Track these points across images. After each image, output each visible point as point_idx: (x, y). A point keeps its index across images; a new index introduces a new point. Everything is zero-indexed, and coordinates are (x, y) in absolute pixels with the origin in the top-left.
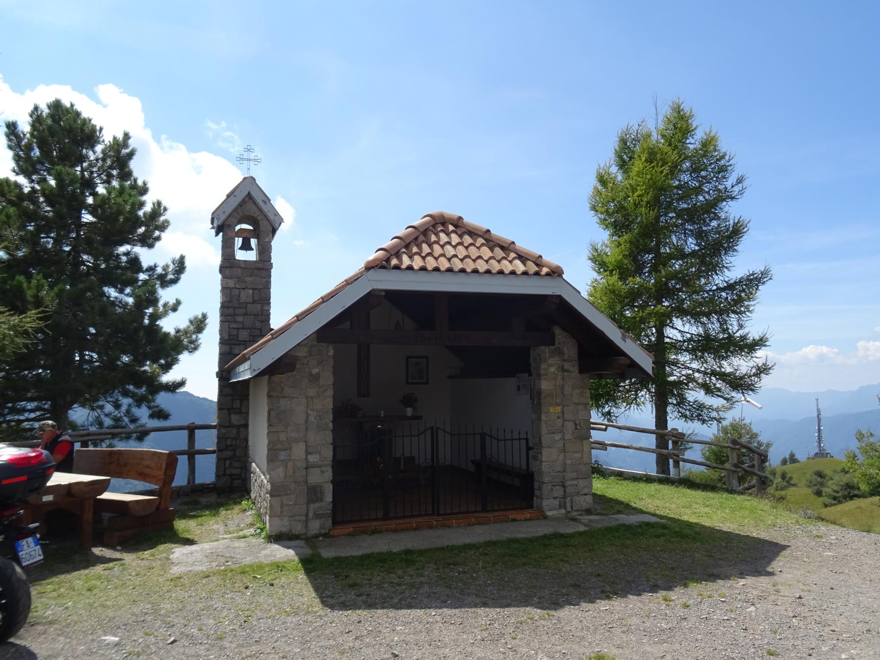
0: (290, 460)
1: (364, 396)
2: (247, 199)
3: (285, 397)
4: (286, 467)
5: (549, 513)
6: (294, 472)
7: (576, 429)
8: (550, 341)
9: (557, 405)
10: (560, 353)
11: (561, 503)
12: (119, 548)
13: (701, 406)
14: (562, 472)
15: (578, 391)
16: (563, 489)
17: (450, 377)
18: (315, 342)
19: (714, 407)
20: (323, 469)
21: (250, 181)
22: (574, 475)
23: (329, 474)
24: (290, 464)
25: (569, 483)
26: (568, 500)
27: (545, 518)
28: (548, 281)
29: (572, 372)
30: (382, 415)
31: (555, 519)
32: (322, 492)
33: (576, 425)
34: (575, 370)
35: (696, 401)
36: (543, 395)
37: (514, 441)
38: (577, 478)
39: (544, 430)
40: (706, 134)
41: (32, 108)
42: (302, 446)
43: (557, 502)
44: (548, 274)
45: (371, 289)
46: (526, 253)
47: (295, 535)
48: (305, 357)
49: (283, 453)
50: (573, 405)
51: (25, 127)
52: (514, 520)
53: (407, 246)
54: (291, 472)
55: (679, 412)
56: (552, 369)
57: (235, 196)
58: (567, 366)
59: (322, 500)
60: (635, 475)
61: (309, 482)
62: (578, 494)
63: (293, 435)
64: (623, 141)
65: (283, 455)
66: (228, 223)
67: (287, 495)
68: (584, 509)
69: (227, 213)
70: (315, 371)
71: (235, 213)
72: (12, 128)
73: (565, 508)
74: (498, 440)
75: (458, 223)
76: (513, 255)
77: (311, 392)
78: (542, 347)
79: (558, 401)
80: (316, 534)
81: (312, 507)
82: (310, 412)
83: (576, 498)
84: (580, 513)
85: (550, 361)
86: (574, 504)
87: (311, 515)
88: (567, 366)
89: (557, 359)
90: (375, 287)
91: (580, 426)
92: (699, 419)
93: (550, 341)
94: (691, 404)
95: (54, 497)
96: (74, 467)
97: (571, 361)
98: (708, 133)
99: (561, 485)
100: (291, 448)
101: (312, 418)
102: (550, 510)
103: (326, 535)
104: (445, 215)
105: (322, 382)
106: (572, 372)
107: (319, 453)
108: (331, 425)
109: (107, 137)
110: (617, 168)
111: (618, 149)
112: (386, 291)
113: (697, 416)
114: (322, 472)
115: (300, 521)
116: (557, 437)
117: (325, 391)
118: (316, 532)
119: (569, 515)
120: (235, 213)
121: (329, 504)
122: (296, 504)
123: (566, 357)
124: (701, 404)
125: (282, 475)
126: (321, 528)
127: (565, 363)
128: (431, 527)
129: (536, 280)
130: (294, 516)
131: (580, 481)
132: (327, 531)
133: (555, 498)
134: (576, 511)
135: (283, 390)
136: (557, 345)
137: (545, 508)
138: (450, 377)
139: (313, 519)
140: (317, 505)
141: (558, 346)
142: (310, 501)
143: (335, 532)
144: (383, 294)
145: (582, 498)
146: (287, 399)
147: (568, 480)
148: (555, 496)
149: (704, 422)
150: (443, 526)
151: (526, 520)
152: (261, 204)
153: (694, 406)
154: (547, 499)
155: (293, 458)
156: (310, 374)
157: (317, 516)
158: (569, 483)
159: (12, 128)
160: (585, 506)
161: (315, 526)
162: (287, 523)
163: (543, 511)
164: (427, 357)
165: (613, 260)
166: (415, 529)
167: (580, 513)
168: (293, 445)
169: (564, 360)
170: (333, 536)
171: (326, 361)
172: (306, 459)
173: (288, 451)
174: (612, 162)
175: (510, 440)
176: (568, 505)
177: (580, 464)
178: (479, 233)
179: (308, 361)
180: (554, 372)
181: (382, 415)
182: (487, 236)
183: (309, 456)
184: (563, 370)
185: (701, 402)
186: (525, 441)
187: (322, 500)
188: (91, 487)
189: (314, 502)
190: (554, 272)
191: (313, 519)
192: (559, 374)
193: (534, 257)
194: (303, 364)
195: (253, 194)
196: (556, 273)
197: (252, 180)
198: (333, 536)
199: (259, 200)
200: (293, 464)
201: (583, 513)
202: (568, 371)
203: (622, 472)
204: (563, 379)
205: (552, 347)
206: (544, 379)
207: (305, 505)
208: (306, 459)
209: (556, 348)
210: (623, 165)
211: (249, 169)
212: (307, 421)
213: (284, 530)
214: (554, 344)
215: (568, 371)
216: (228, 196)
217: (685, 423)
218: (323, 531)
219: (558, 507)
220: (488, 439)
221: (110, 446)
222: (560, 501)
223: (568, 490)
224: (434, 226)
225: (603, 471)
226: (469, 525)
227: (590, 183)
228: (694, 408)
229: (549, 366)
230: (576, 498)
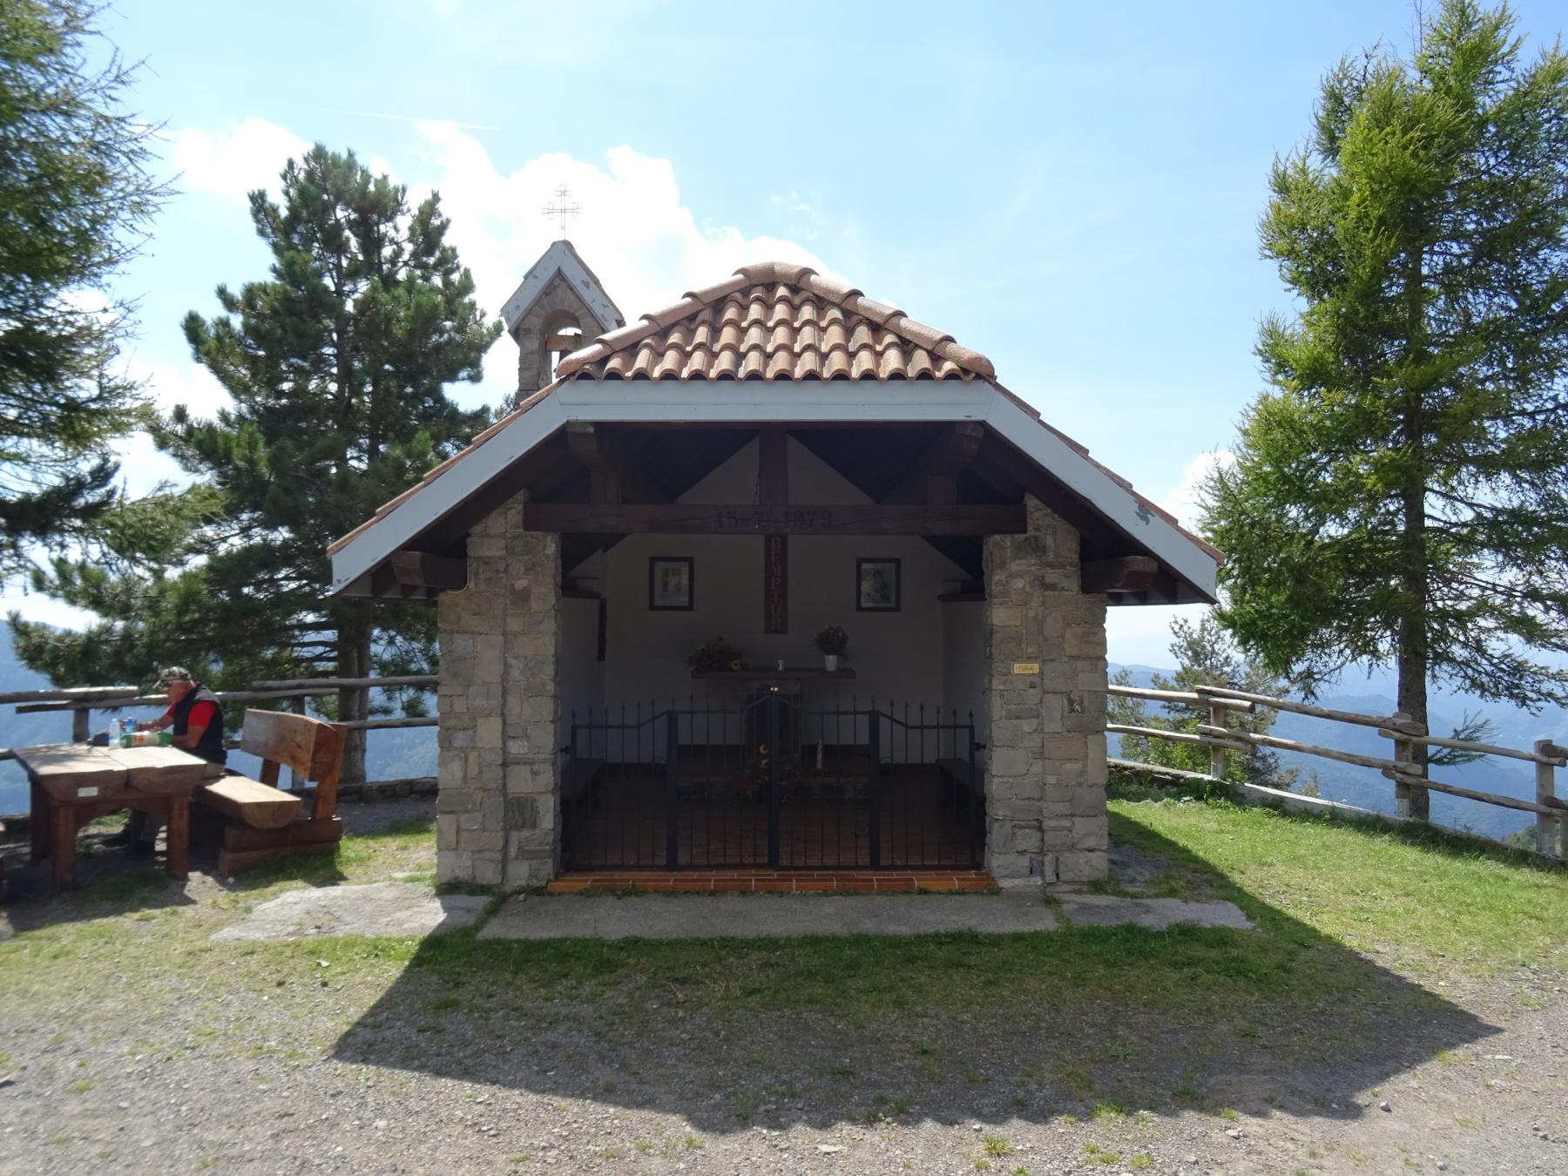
0: (474, 748)
1: (776, 632)
2: (557, 282)
3: (465, 632)
4: (466, 760)
5: (1005, 884)
6: (480, 772)
7: (1072, 710)
8: (1018, 524)
9: (1030, 659)
10: (1038, 548)
11: (1035, 863)
12: (231, 880)
13: (1519, 669)
14: (1038, 800)
15: (1079, 630)
16: (1039, 835)
17: (943, 598)
18: (521, 530)
19: (1550, 671)
20: (535, 767)
21: (564, 248)
22: (1064, 808)
23: (547, 778)
24: (473, 756)
25: (1053, 823)
26: (1049, 858)
27: (996, 892)
28: (954, 390)
29: (1063, 589)
30: (781, 668)
31: (1019, 897)
32: (535, 812)
33: (1071, 702)
34: (1073, 585)
35: (1507, 656)
36: (996, 638)
37: (926, 731)
38: (1072, 815)
39: (997, 707)
40: (1544, 56)
41: (284, 166)
42: (496, 723)
43: (1024, 862)
44: (951, 376)
45: (564, 421)
46: (917, 334)
47: (483, 886)
48: (501, 558)
49: (460, 735)
50: (1065, 659)
51: (279, 201)
52: (923, 892)
53: (664, 334)
54: (476, 771)
55: (1466, 677)
56: (1019, 584)
57: (535, 277)
58: (1052, 576)
59: (534, 826)
60: (1309, 807)
61: (510, 791)
62: (1072, 848)
63: (477, 703)
64: (1335, 97)
65: (460, 740)
66: (523, 326)
67: (466, 811)
68: (1086, 879)
69: (523, 308)
70: (521, 584)
71: (537, 308)
72: (259, 203)
73: (1042, 874)
74: (907, 727)
75: (799, 286)
76: (889, 338)
77: (514, 624)
78: (997, 537)
79: (1030, 650)
80: (522, 887)
81: (515, 836)
82: (512, 662)
83: (1066, 857)
84: (1077, 887)
85: (1014, 567)
86: (1062, 867)
87: (513, 851)
88: (1052, 576)
89: (1033, 561)
90: (573, 418)
91: (1081, 704)
92: (1511, 696)
93: (1018, 524)
94: (1495, 661)
95: (100, 791)
96: (314, 732)
97: (1063, 566)
98: (1551, 52)
99: (1034, 827)
100: (475, 726)
101: (515, 673)
102: (1007, 876)
103: (539, 891)
104: (777, 268)
105: (534, 605)
106: (1063, 589)
107: (528, 737)
108: (551, 687)
109: (414, 202)
110: (1321, 157)
111: (1321, 114)
112: (600, 426)
113: (1507, 688)
114: (535, 773)
115: (492, 861)
116: (1027, 726)
117: (540, 623)
118: (523, 883)
119: (1050, 889)
120: (537, 308)
121: (546, 834)
122: (484, 830)
123: (1050, 557)
124: (1520, 664)
125: (459, 775)
126: (531, 876)
127: (1049, 570)
128: (745, 892)
129: (925, 390)
130: (480, 851)
131: (1078, 821)
132: (543, 883)
133: (1023, 853)
134: (1065, 882)
135: (459, 619)
136: (1031, 532)
137: (996, 873)
138: (943, 598)
139: (517, 858)
140: (525, 833)
141: (1033, 533)
142: (508, 828)
143: (559, 886)
144: (591, 430)
145: (1082, 858)
146: (466, 636)
147: (1050, 818)
148: (1021, 848)
149: (1523, 701)
150: (769, 892)
151: (951, 893)
152: (580, 288)
153: (1503, 666)
154: (1000, 853)
155: (479, 745)
156: (513, 591)
157: (524, 854)
158: (1053, 823)
159: (259, 203)
160: (1087, 873)
161: (520, 873)
162: (469, 863)
163: (993, 879)
164: (897, 561)
165: (1304, 357)
166: (713, 893)
167: (1077, 887)
168: (479, 721)
169: (1048, 565)
170: (551, 894)
171: (541, 565)
172: (504, 748)
173: (471, 732)
174: (1311, 146)
175: (927, 727)
176: (1049, 870)
177: (1080, 785)
178: (833, 299)
179: (507, 566)
180: (1024, 588)
181: (781, 668)
182: (848, 305)
183: (510, 743)
184: (1045, 586)
185: (1519, 660)
186: (967, 731)
187: (534, 826)
188: (170, 777)
189: (520, 828)
190: (966, 371)
191: (517, 858)
192: (1036, 593)
193: (929, 339)
194: (498, 571)
195: (567, 271)
196: (977, 373)
197: (564, 248)
198: (551, 894)
199: (575, 279)
200: (480, 756)
201: (1085, 888)
202: (1053, 587)
203: (1282, 799)
204: (1043, 604)
205: (1021, 537)
206: (1001, 604)
207: (501, 834)
208: (504, 748)
209: (1027, 539)
210: (1331, 147)
211: (563, 228)
212: (505, 676)
213: (463, 875)
214: (1025, 531)
215: (1053, 587)
216: (526, 277)
217: (1482, 701)
218: (535, 883)
219: (1027, 872)
220: (884, 724)
221: (1025, 669)
222: (1031, 860)
223: (1050, 838)
224: (746, 292)
225: (1242, 795)
226: (825, 894)
227: (1259, 200)
228: (1503, 670)
229: (1011, 576)
230: (1066, 857)
